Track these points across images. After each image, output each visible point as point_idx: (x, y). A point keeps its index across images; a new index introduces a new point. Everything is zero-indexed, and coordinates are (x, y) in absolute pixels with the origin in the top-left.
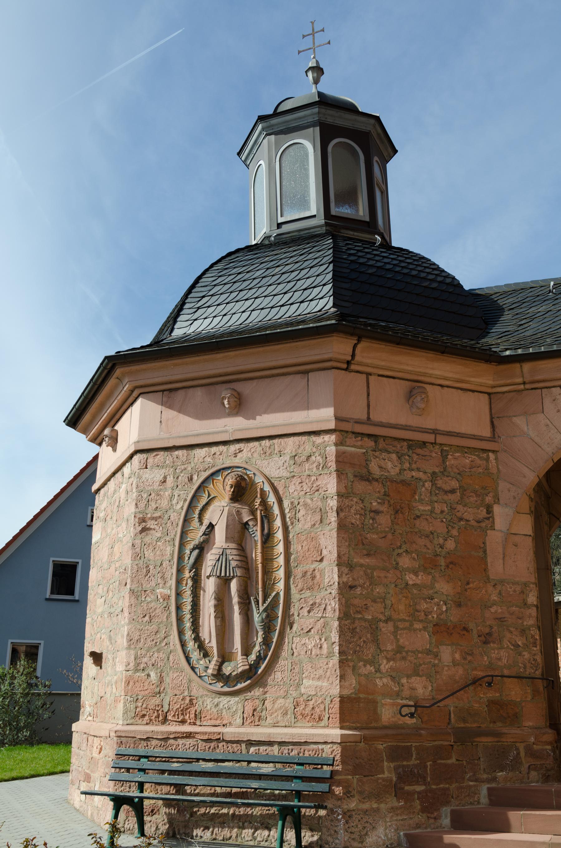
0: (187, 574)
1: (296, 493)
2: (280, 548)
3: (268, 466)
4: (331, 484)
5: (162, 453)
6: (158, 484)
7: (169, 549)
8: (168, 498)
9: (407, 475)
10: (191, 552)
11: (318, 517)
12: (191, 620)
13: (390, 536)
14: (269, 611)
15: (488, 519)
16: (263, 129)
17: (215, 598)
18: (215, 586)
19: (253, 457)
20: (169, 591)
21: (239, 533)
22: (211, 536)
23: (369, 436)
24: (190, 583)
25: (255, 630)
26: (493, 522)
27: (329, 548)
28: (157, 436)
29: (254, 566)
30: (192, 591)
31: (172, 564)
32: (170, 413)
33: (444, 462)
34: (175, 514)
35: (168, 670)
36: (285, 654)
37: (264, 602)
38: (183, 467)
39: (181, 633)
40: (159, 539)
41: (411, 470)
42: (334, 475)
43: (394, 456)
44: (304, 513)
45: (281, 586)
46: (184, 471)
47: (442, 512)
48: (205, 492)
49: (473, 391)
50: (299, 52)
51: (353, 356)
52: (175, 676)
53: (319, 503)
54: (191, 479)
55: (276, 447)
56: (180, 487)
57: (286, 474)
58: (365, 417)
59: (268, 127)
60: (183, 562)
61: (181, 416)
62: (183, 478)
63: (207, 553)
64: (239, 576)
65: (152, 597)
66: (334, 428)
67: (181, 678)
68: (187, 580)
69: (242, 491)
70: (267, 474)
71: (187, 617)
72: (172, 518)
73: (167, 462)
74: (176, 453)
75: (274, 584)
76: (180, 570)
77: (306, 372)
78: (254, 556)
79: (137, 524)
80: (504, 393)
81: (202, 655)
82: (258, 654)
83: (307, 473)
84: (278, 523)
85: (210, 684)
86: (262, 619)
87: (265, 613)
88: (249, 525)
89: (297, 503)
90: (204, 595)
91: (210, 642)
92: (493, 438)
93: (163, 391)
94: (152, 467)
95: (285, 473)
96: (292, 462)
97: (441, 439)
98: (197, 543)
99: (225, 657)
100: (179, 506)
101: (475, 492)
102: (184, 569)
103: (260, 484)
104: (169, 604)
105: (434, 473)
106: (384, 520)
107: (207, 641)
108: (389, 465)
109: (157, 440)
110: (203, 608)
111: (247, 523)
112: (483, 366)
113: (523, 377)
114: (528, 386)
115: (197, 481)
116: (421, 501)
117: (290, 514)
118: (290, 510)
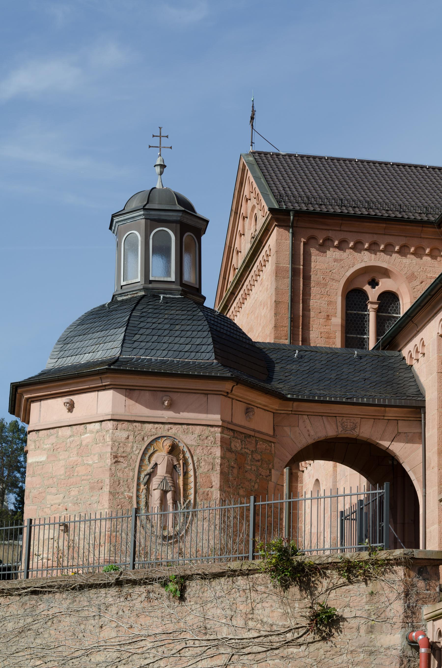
0: (142, 487)
3: (187, 439)
4: (218, 452)
5: (126, 423)
6: (124, 439)
7: (131, 474)
9: (244, 450)
11: (211, 467)
13: (237, 479)
15: (270, 475)
16: (143, 215)
21: (172, 469)
22: (155, 469)
23: (232, 430)
24: (145, 491)
26: (271, 478)
27: (216, 482)
28: (122, 413)
32: (130, 402)
33: (256, 446)
37: (184, 504)
38: (139, 432)
40: (125, 468)
41: (245, 448)
42: (220, 448)
43: (239, 441)
44: (204, 464)
47: (254, 470)
49: (268, 411)
50: (150, 147)
51: (232, 391)
53: (212, 460)
55: (190, 429)
57: (195, 444)
58: (230, 421)
59: (147, 215)
61: (137, 404)
62: (139, 438)
65: (122, 496)
66: (221, 424)
69: (174, 450)
70: (185, 442)
73: (130, 428)
74: (135, 424)
76: (138, 485)
77: (207, 394)
79: (112, 459)
80: (280, 413)
83: (206, 445)
84: (191, 467)
92: (274, 436)
93: (126, 389)
94: (121, 429)
96: (198, 438)
97: (257, 435)
98: (149, 472)
100: (137, 452)
101: (266, 462)
105: (253, 451)
106: (235, 471)
108: (238, 445)
109: (122, 415)
111: (176, 465)
112: (277, 400)
113: (293, 408)
114: (293, 413)
116: (247, 464)
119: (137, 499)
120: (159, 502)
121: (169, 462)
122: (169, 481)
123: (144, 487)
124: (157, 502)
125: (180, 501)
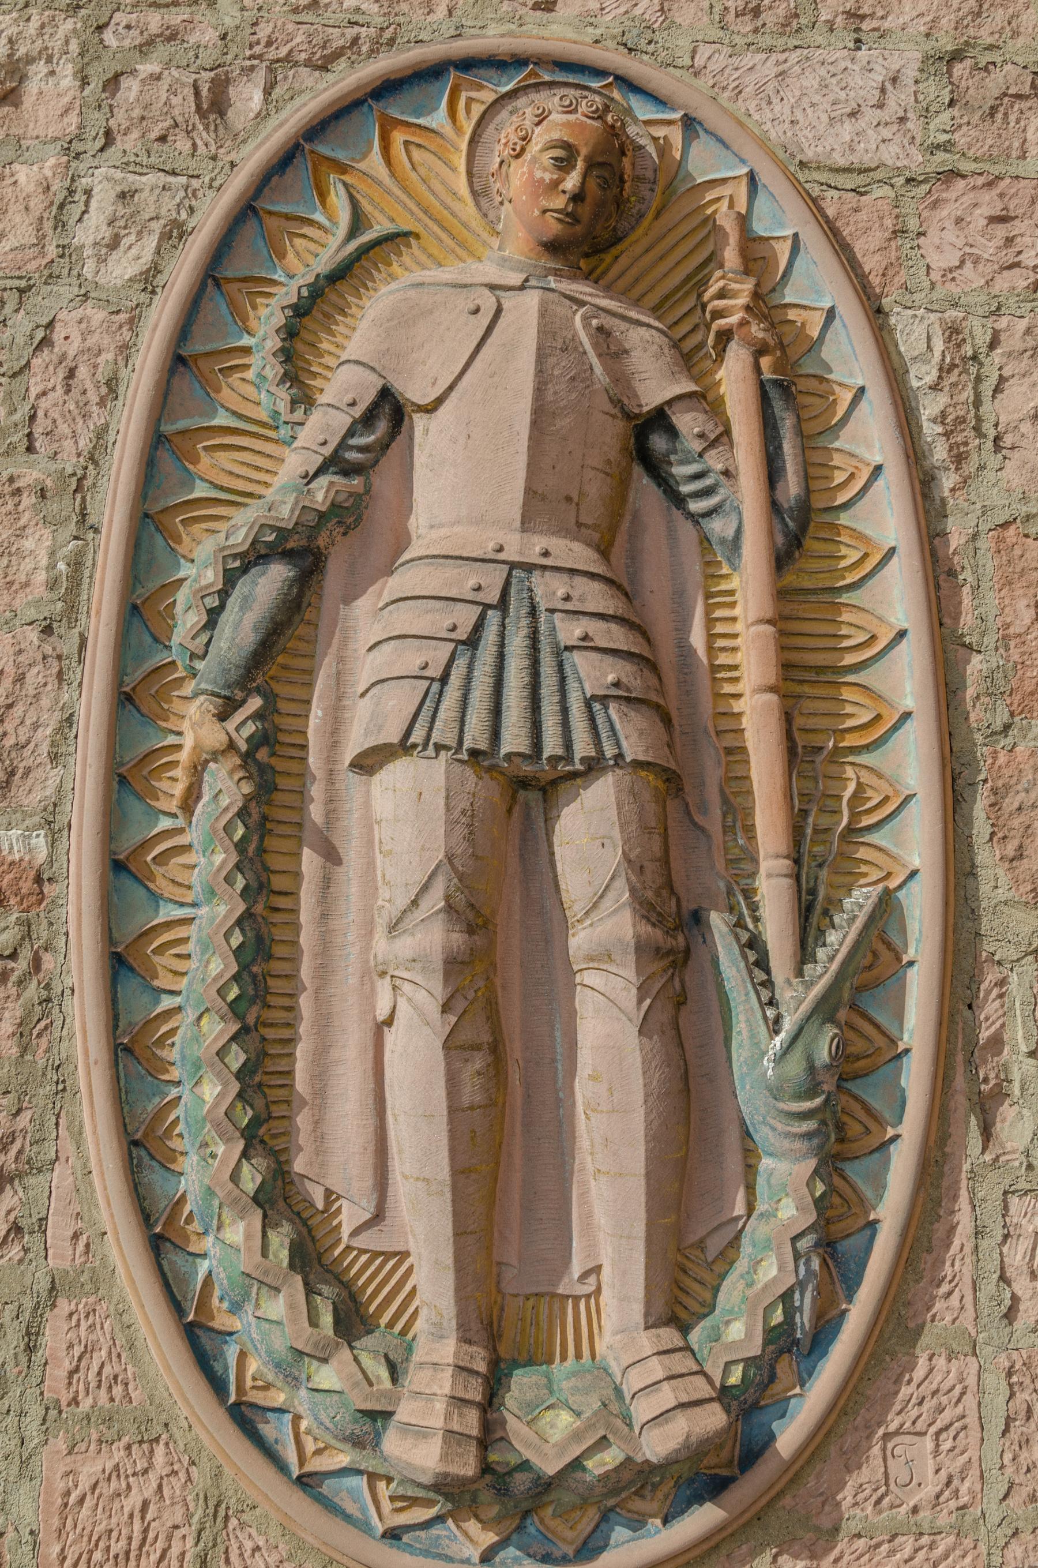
0: (194, 725)
1: (972, 277)
2: (895, 599)
7: (39, 550)
8: (37, 204)
10: (230, 579)
12: (237, 1058)
14: (842, 1015)
17: (450, 908)
18: (451, 824)
19: (670, 25)
20: (40, 842)
21: (623, 467)
22: (383, 481)
24: (225, 788)
25: (732, 1139)
29: (706, 705)
30: (241, 847)
31: (69, 646)
34: (98, 316)
35: (32, 1429)
36: (950, 1310)
37: (804, 954)
39: (143, 1147)
45: (913, 843)
46: (162, 51)
48: (323, 196)
52: (89, 1471)
54: (214, 105)
56: (129, 143)
57: (896, 153)
60: (161, 641)
62: (158, 89)
63: (349, 598)
64: (637, 764)
67: (144, 1489)
68: (197, 770)
69: (613, 217)
71: (197, 1035)
72: (69, 339)
75: (851, 830)
76: (133, 700)
78: (697, 639)
81: (327, 1319)
82: (778, 1316)
84: (868, 438)
85: (393, 1535)
86: (811, 1069)
87: (830, 1031)
88: (672, 432)
89: (983, 338)
90: (326, 882)
91: (378, 1217)
95: (894, 149)
98: (285, 513)
99: (508, 1329)
100: (123, 267)
102: (163, 695)
103: (726, 191)
104: (42, 932)
107: (350, 1216)
110: (324, 971)
111: (659, 419)
115: (263, 123)
117: (942, 400)
118: (945, 370)
119: (110, 911)
120: (431, 937)
121: (560, 366)
122: (570, 631)
123: (214, 736)
124: (406, 946)
125: (742, 895)
